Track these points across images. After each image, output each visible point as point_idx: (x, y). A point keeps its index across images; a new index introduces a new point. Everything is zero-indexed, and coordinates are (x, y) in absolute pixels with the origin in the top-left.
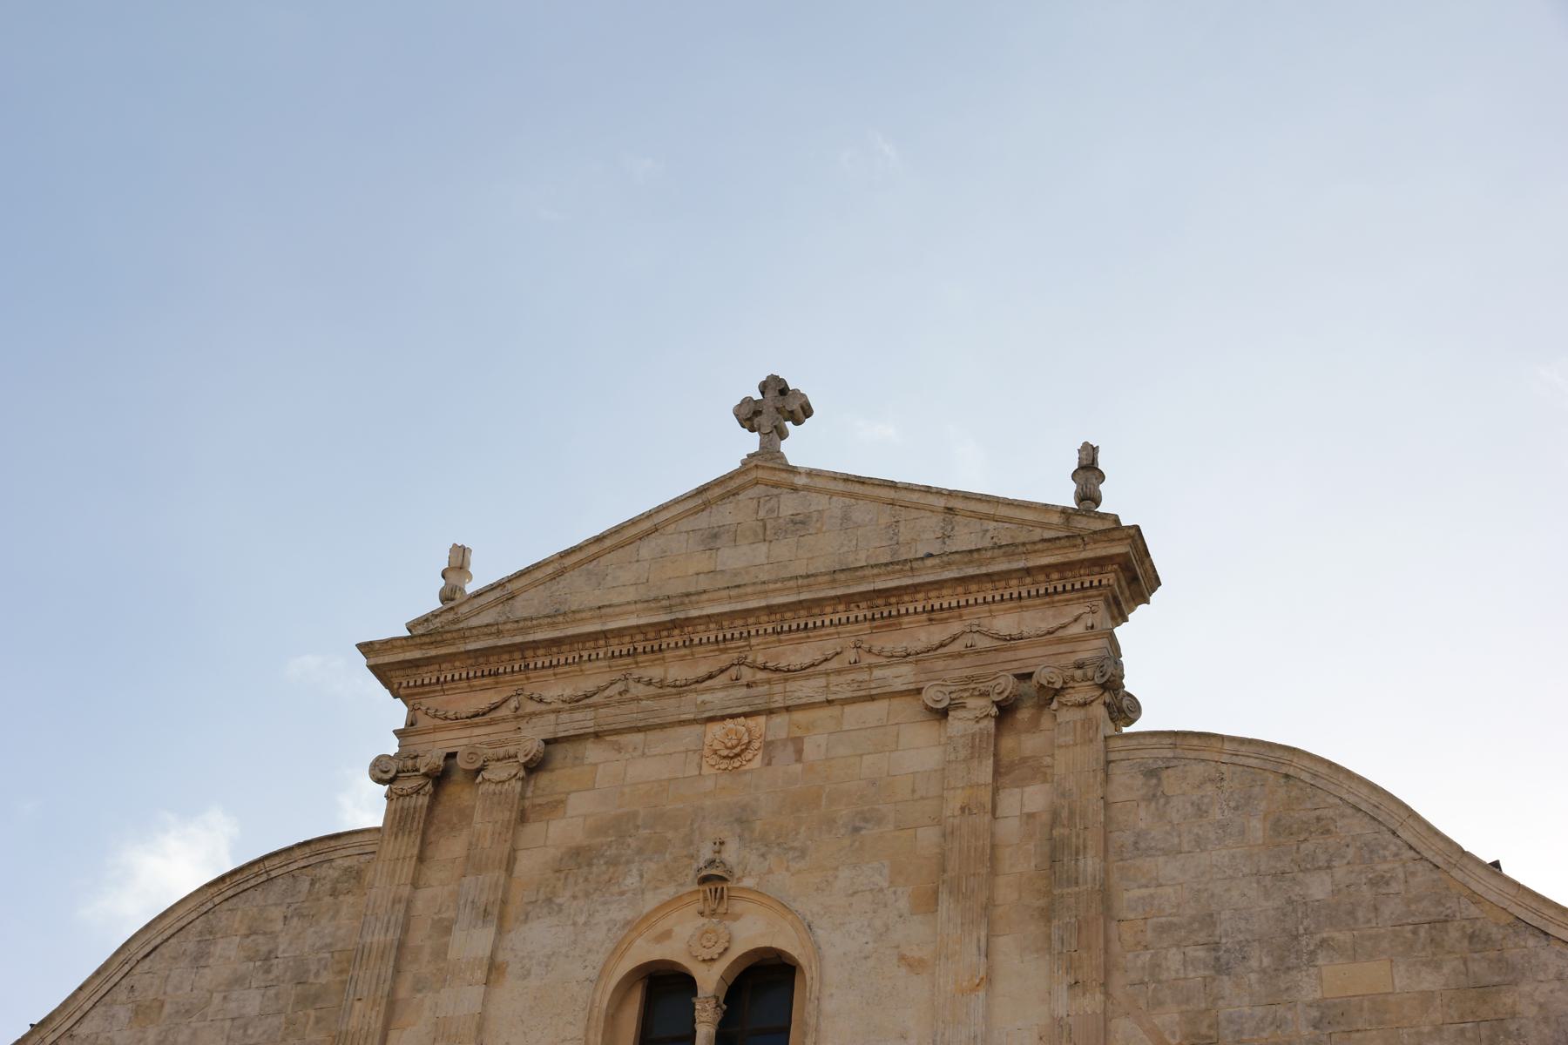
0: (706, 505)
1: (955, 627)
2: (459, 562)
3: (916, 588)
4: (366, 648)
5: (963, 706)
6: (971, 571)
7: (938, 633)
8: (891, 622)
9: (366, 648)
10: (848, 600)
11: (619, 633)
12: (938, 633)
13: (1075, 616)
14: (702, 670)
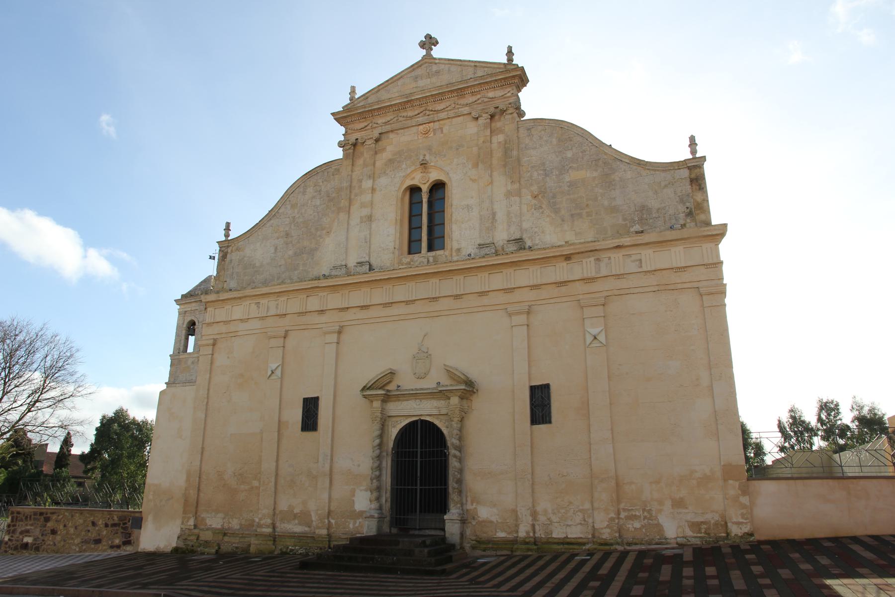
0: (414, 70)
1: (479, 96)
2: (353, 90)
3: (468, 87)
4: (333, 114)
5: (482, 116)
6: (482, 81)
7: (474, 98)
8: (462, 96)
9: (333, 114)
10: (452, 91)
11: (395, 105)
12: (474, 98)
13: (508, 91)
14: (416, 113)
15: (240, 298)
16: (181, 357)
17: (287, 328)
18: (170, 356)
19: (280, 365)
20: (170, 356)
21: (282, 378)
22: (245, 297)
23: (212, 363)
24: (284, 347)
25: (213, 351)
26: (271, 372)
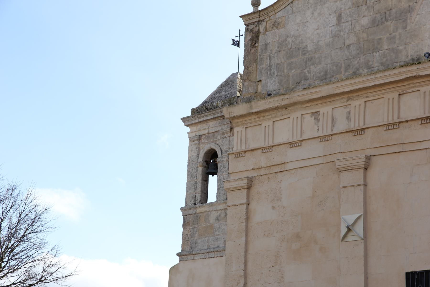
15: (285, 107)
16: (199, 210)
17: (369, 152)
18: (182, 209)
19: (359, 218)
20: (182, 209)
21: (365, 238)
22: (294, 104)
23: (248, 219)
24: (365, 185)
25: (248, 197)
26: (346, 229)
